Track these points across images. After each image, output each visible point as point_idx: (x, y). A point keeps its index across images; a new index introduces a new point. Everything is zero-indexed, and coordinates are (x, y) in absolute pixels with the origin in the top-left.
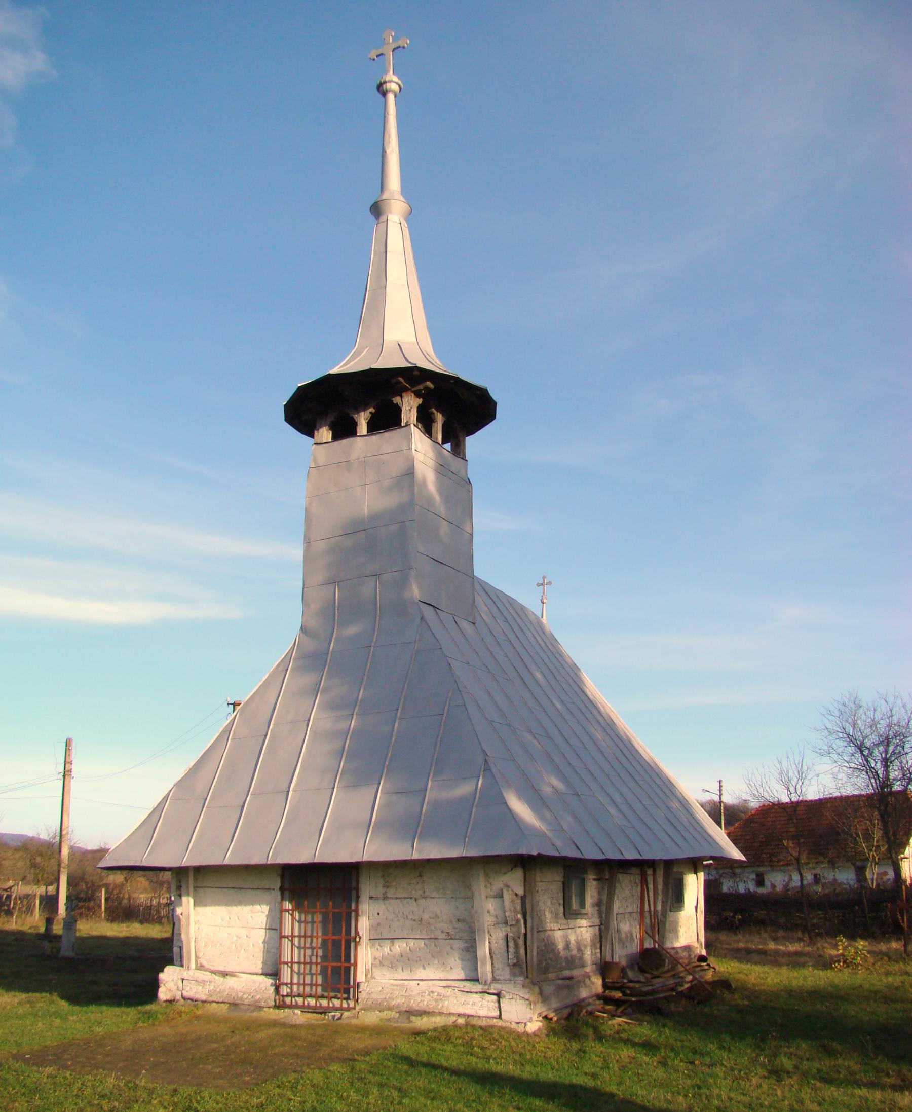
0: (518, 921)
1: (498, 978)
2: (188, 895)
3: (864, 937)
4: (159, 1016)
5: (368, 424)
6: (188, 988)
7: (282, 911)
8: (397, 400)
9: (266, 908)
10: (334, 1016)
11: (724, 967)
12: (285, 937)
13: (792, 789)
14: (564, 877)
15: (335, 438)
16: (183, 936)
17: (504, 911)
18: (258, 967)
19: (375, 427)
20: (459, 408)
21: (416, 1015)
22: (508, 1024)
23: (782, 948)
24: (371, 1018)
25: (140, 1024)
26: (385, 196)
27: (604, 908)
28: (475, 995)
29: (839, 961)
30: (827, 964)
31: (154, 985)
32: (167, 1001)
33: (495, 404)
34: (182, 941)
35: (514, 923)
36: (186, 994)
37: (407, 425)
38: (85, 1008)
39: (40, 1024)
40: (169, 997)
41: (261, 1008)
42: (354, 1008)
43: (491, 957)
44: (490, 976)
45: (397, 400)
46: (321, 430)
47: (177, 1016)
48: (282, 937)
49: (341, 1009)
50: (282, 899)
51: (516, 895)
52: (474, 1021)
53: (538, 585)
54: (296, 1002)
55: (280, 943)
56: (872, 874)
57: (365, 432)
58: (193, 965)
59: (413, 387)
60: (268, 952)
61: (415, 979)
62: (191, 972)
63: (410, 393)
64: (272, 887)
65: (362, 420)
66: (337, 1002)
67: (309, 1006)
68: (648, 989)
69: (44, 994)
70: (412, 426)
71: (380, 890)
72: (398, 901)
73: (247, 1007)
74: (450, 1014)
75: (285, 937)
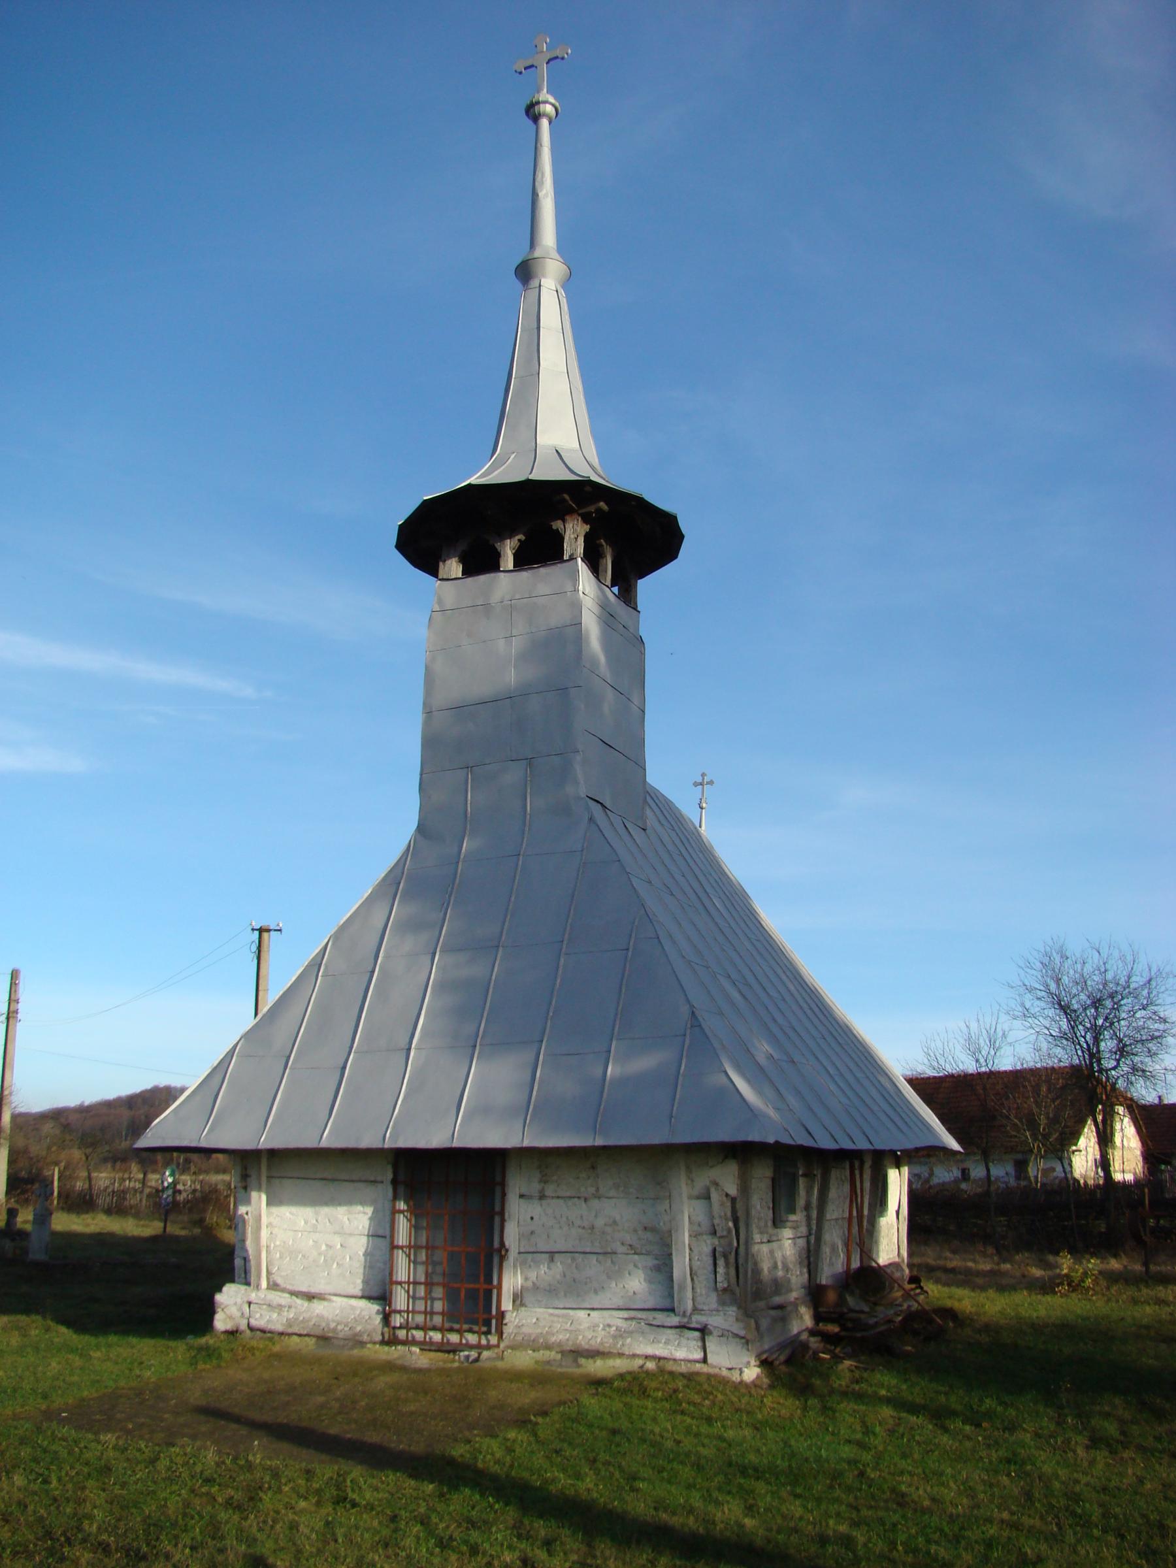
0: (729, 1231)
1: (700, 1307)
2: (259, 1189)
3: (1093, 1255)
4: (225, 1355)
5: (515, 556)
6: (258, 1316)
7: (394, 1212)
8: (557, 525)
9: (369, 1210)
10: (467, 1357)
11: (935, 1292)
12: (398, 1247)
13: (982, 1060)
14: (775, 1171)
15: (467, 572)
16: (249, 1243)
17: (712, 1217)
18: (357, 1287)
19: (523, 560)
20: (634, 537)
21: (587, 1357)
22: (716, 1371)
23: (970, 1264)
24: (524, 1360)
25: (201, 1366)
26: (537, 254)
27: (814, 1214)
28: (669, 1331)
29: (1062, 1284)
30: (1046, 1287)
31: (209, 1310)
32: (226, 1332)
33: (682, 537)
34: (247, 1251)
35: (725, 1233)
36: (253, 1322)
37: (572, 558)
38: (101, 1339)
39: (54, 1364)
40: (229, 1326)
41: (362, 1344)
42: (498, 1346)
43: (692, 1279)
44: (689, 1305)
45: (557, 525)
46: (448, 562)
47: (249, 1354)
48: (393, 1247)
49: (478, 1346)
50: (395, 1197)
51: (727, 1195)
52: (670, 1366)
53: (696, 784)
54: (413, 1336)
55: (392, 1255)
56: (1035, 1170)
57: (511, 566)
58: (264, 1284)
59: (580, 505)
60: (371, 1267)
61: (580, 1309)
62: (261, 1294)
63: (575, 516)
64: (379, 1178)
65: (508, 552)
66: (472, 1338)
67: (431, 1343)
68: (857, 1323)
69: (34, 1317)
70: (579, 560)
71: (536, 1187)
72: (561, 1201)
73: (342, 1343)
74: (634, 1356)
75: (398, 1247)
